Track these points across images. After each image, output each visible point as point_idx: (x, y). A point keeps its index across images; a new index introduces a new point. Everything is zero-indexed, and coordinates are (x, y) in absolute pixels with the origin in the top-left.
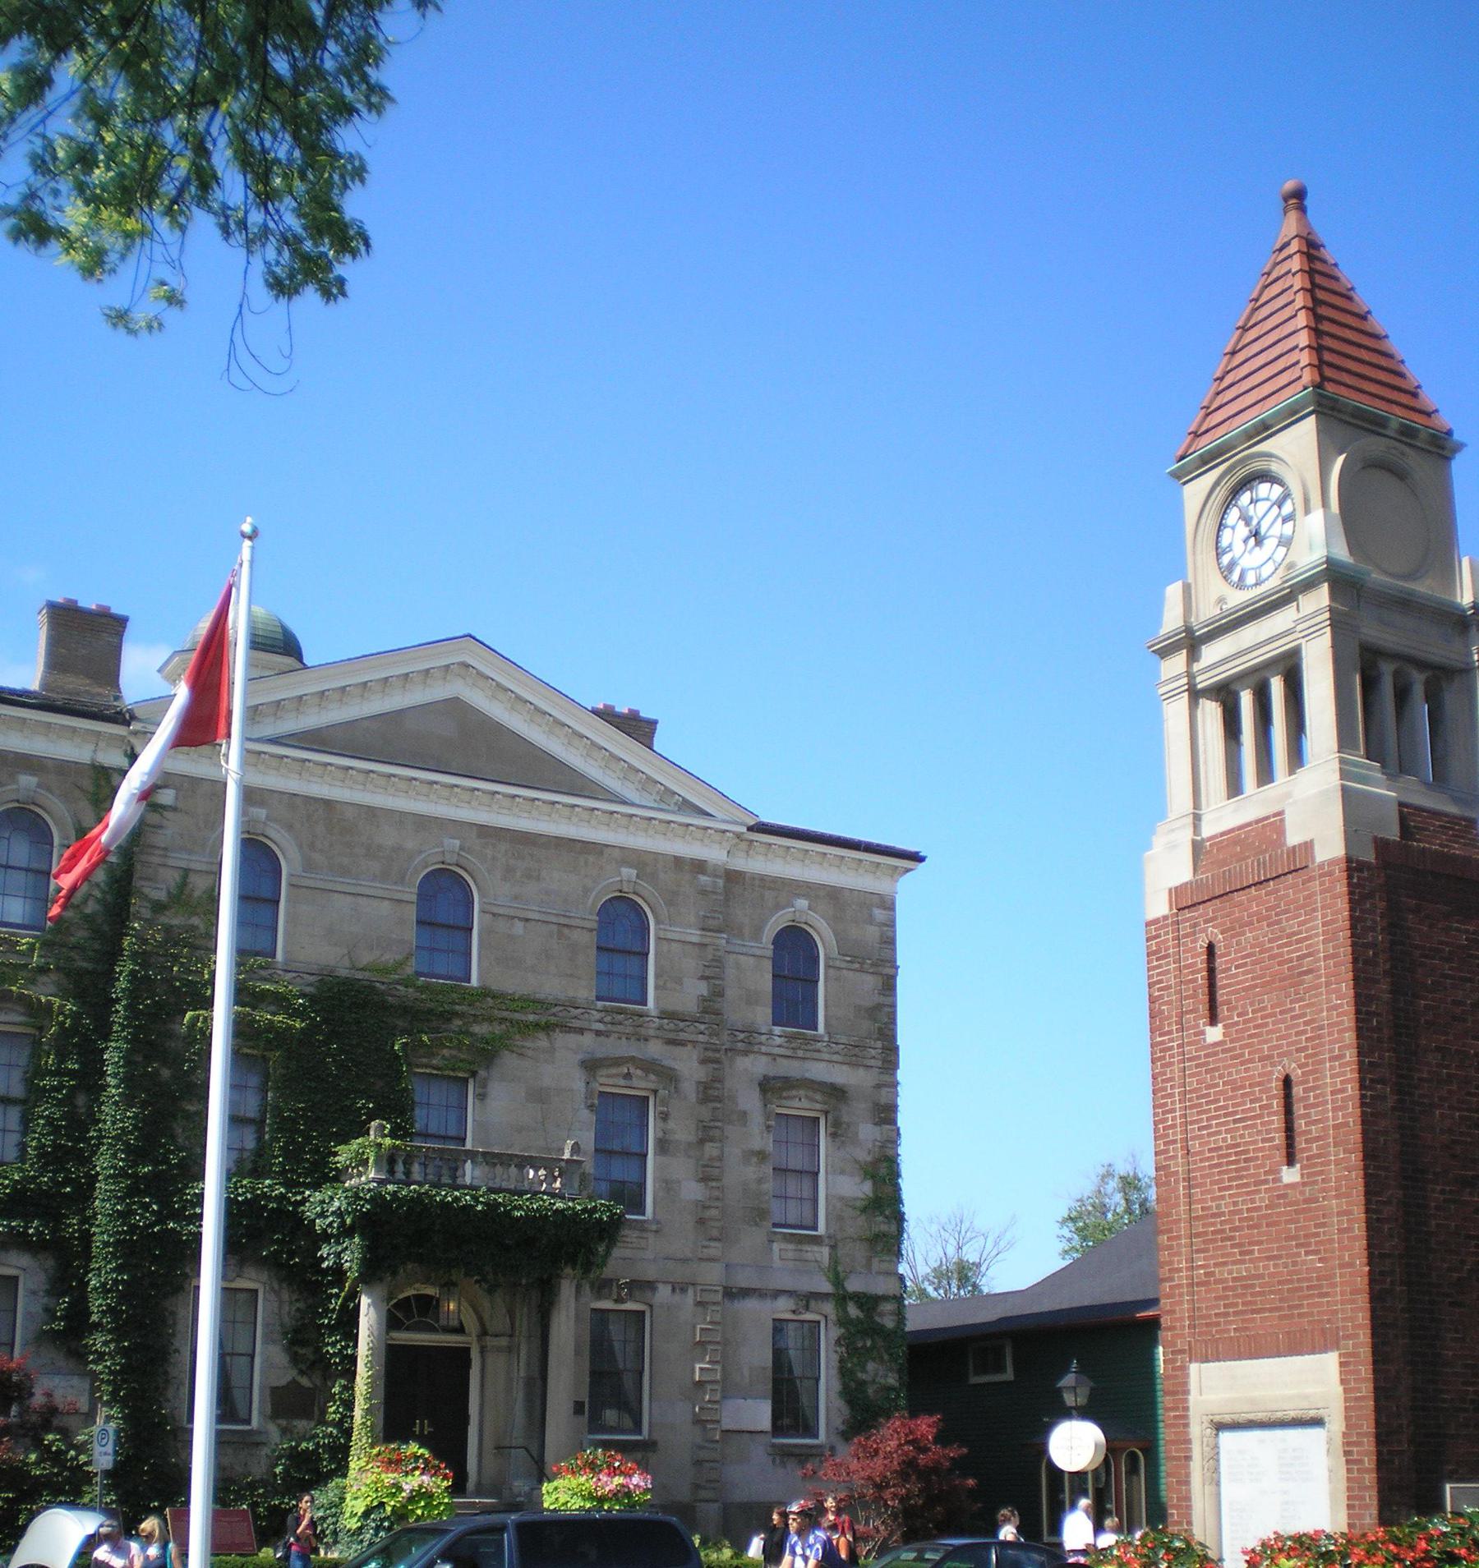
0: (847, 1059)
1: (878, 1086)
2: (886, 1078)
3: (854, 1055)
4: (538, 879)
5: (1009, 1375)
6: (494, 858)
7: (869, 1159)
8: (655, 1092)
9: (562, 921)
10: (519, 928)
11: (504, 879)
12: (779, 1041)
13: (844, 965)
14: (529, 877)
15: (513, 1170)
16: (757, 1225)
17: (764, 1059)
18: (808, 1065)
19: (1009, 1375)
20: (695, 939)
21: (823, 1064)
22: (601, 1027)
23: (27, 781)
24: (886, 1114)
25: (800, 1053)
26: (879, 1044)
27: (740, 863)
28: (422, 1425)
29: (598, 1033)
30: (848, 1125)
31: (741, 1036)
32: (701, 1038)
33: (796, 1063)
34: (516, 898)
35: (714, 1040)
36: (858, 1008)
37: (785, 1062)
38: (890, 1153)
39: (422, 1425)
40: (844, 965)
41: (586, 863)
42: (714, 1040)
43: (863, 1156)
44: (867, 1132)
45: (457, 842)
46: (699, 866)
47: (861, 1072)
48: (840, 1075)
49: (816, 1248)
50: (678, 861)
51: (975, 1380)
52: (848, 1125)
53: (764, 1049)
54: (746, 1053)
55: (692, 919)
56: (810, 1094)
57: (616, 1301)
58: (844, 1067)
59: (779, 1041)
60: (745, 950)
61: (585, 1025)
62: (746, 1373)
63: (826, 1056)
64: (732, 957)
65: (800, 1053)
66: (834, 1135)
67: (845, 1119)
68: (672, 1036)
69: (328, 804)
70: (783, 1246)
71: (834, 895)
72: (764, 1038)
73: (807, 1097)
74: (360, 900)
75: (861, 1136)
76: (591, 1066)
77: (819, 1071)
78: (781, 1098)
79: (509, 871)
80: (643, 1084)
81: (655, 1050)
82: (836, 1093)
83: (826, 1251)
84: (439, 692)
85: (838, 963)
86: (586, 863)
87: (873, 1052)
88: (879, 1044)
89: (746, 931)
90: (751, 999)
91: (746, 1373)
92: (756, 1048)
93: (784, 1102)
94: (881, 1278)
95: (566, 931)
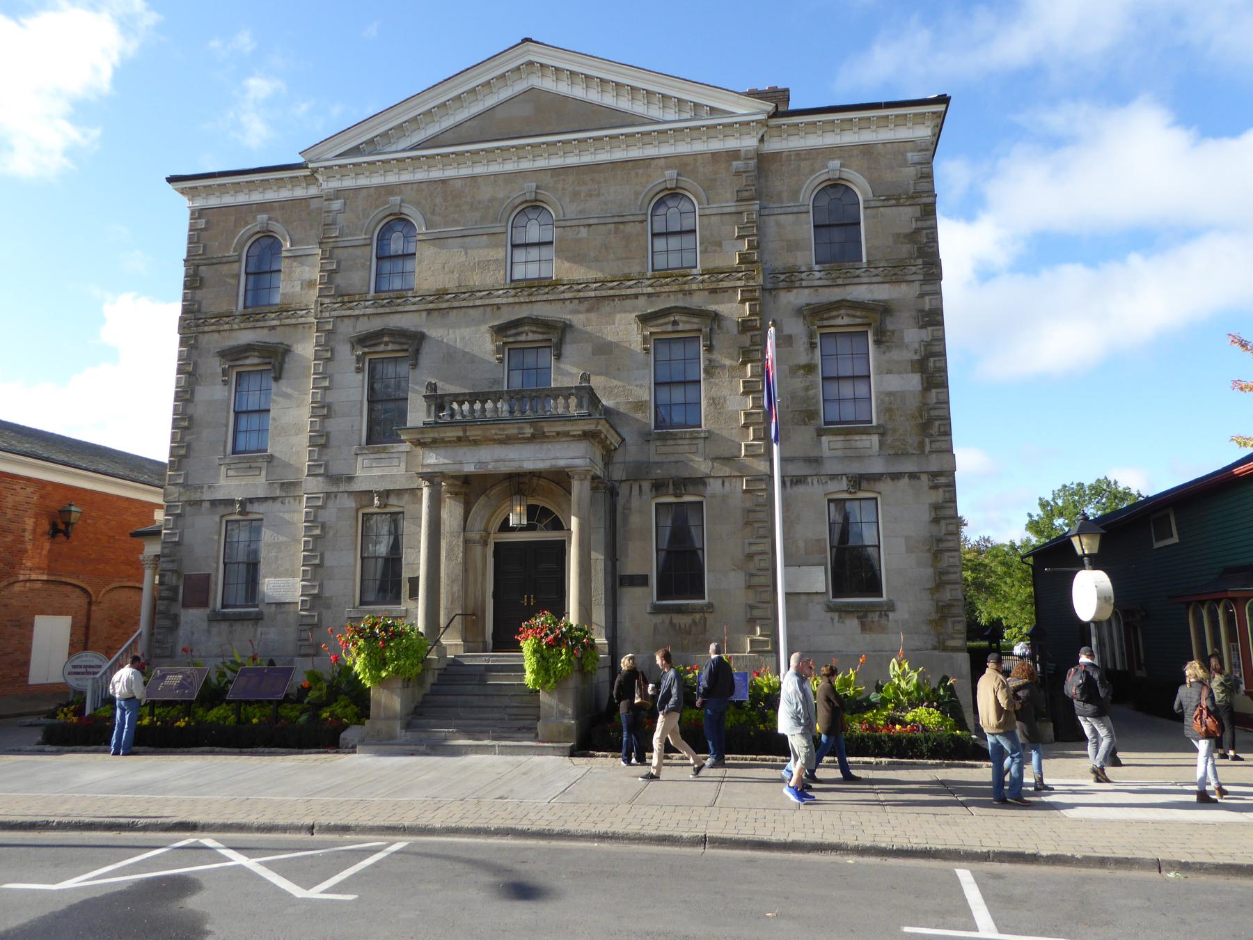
0: (888, 279)
1: (922, 296)
2: (928, 288)
3: (895, 272)
4: (598, 195)
5: (1175, 539)
6: (563, 189)
7: (917, 357)
8: (700, 330)
9: (616, 220)
10: (584, 232)
11: (572, 201)
12: (818, 275)
13: (879, 204)
14: (591, 196)
15: (561, 400)
16: (805, 424)
17: (806, 291)
18: (849, 289)
19: (1175, 539)
20: (733, 210)
21: (865, 287)
22: (650, 290)
23: (262, 217)
24: (933, 318)
25: (840, 281)
26: (920, 261)
27: (774, 145)
28: (529, 598)
29: (649, 295)
30: (893, 332)
31: (783, 277)
32: (739, 283)
33: (836, 290)
34: (580, 212)
35: (751, 283)
36: (898, 235)
37: (827, 290)
38: (937, 349)
39: (529, 598)
40: (879, 204)
41: (637, 174)
42: (751, 283)
43: (910, 355)
44: (913, 336)
45: (534, 185)
46: (734, 154)
47: (904, 287)
48: (882, 293)
49: (864, 437)
50: (715, 156)
51: (1157, 545)
52: (893, 332)
53: (804, 283)
54: (789, 289)
55: (729, 195)
56: (851, 312)
57: (676, 496)
58: (887, 286)
59: (818, 275)
60: (782, 211)
61: (639, 291)
62: (801, 545)
63: (866, 280)
64: (772, 218)
65: (840, 281)
66: (878, 342)
67: (890, 327)
68: (714, 286)
69: (443, 181)
70: (831, 438)
71: (867, 150)
72: (804, 276)
73: (848, 315)
74: (466, 239)
75: (907, 340)
76: (645, 319)
77: (861, 293)
78: (822, 319)
79: (576, 194)
80: (688, 327)
81: (697, 301)
82: (884, 310)
83: (875, 439)
84: (520, 86)
85: (873, 204)
86: (637, 174)
87: (914, 269)
88: (920, 261)
89: (785, 195)
90: (793, 246)
91: (801, 545)
92: (797, 284)
93: (826, 323)
94: (934, 456)
95: (621, 227)
